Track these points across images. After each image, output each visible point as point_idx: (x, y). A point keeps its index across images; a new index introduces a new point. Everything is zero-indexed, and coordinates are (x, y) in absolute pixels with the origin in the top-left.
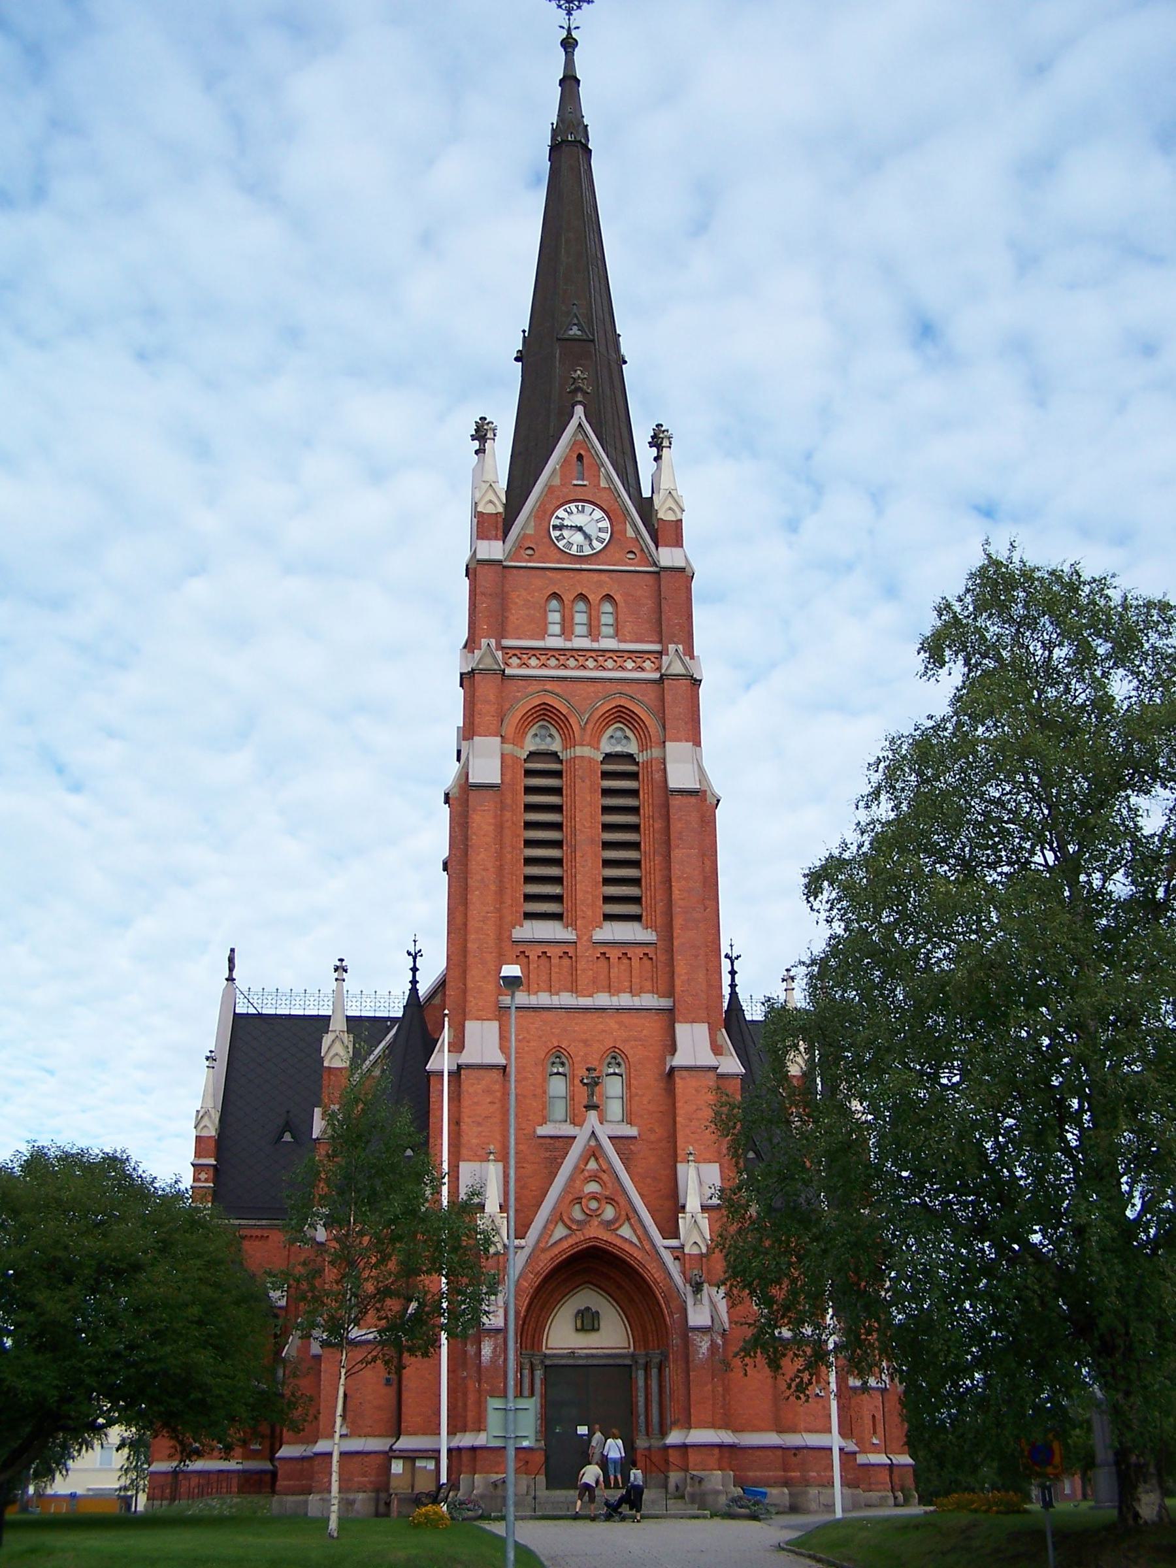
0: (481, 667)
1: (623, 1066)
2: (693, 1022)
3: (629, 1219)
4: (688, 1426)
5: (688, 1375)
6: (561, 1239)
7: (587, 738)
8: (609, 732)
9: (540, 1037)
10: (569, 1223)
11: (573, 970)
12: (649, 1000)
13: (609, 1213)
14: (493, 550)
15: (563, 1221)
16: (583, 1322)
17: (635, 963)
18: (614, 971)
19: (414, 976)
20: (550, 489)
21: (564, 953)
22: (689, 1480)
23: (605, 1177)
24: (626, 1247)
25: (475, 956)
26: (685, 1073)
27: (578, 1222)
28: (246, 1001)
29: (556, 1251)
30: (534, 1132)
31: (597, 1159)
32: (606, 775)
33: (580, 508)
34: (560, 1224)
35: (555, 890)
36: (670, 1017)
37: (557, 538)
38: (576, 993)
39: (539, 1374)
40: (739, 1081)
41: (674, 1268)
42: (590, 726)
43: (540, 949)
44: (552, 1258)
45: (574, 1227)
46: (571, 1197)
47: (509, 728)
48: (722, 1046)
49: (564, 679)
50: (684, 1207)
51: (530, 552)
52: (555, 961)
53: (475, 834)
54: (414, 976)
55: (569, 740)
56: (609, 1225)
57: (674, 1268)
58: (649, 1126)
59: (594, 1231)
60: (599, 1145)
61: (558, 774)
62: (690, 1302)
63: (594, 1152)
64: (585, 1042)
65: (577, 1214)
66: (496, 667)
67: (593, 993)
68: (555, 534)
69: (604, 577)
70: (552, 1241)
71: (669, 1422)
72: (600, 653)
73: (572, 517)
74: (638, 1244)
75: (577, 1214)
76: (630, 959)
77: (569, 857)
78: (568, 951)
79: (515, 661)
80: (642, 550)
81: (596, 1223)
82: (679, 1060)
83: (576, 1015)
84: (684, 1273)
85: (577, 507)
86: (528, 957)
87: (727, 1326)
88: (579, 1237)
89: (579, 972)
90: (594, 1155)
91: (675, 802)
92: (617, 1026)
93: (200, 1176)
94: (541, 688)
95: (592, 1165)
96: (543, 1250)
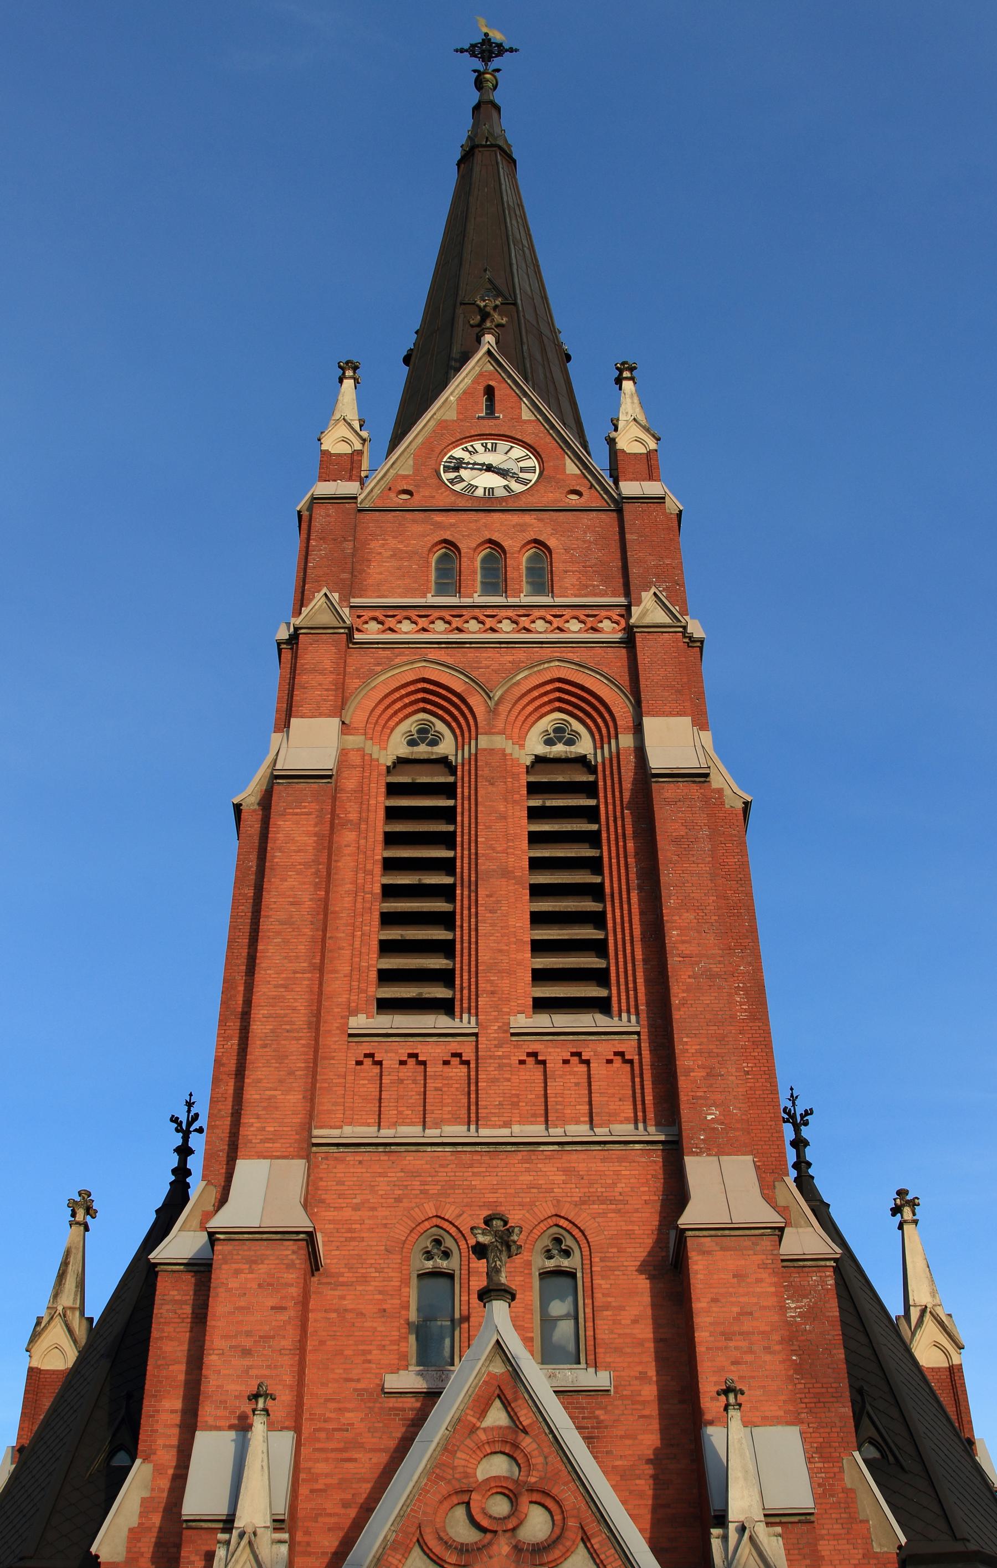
5: (304, 586)
8: (548, 722)
9: (399, 1200)
10: (438, 1549)
15: (422, 1543)
19: (183, 1162)
25: (265, 1046)
31: (506, 1405)
33: (489, 446)
34: (416, 1552)
35: (437, 963)
37: (452, 481)
40: (830, 1273)
46: (444, 1488)
53: (280, 850)
58: (640, 1368)
61: (449, 790)
68: (446, 477)
69: (528, 518)
72: (522, 612)
75: (462, 1531)
83: (476, 1157)
86: (380, 1063)
90: (502, 1397)
91: (663, 793)
92: (560, 1178)
95: (497, 1417)
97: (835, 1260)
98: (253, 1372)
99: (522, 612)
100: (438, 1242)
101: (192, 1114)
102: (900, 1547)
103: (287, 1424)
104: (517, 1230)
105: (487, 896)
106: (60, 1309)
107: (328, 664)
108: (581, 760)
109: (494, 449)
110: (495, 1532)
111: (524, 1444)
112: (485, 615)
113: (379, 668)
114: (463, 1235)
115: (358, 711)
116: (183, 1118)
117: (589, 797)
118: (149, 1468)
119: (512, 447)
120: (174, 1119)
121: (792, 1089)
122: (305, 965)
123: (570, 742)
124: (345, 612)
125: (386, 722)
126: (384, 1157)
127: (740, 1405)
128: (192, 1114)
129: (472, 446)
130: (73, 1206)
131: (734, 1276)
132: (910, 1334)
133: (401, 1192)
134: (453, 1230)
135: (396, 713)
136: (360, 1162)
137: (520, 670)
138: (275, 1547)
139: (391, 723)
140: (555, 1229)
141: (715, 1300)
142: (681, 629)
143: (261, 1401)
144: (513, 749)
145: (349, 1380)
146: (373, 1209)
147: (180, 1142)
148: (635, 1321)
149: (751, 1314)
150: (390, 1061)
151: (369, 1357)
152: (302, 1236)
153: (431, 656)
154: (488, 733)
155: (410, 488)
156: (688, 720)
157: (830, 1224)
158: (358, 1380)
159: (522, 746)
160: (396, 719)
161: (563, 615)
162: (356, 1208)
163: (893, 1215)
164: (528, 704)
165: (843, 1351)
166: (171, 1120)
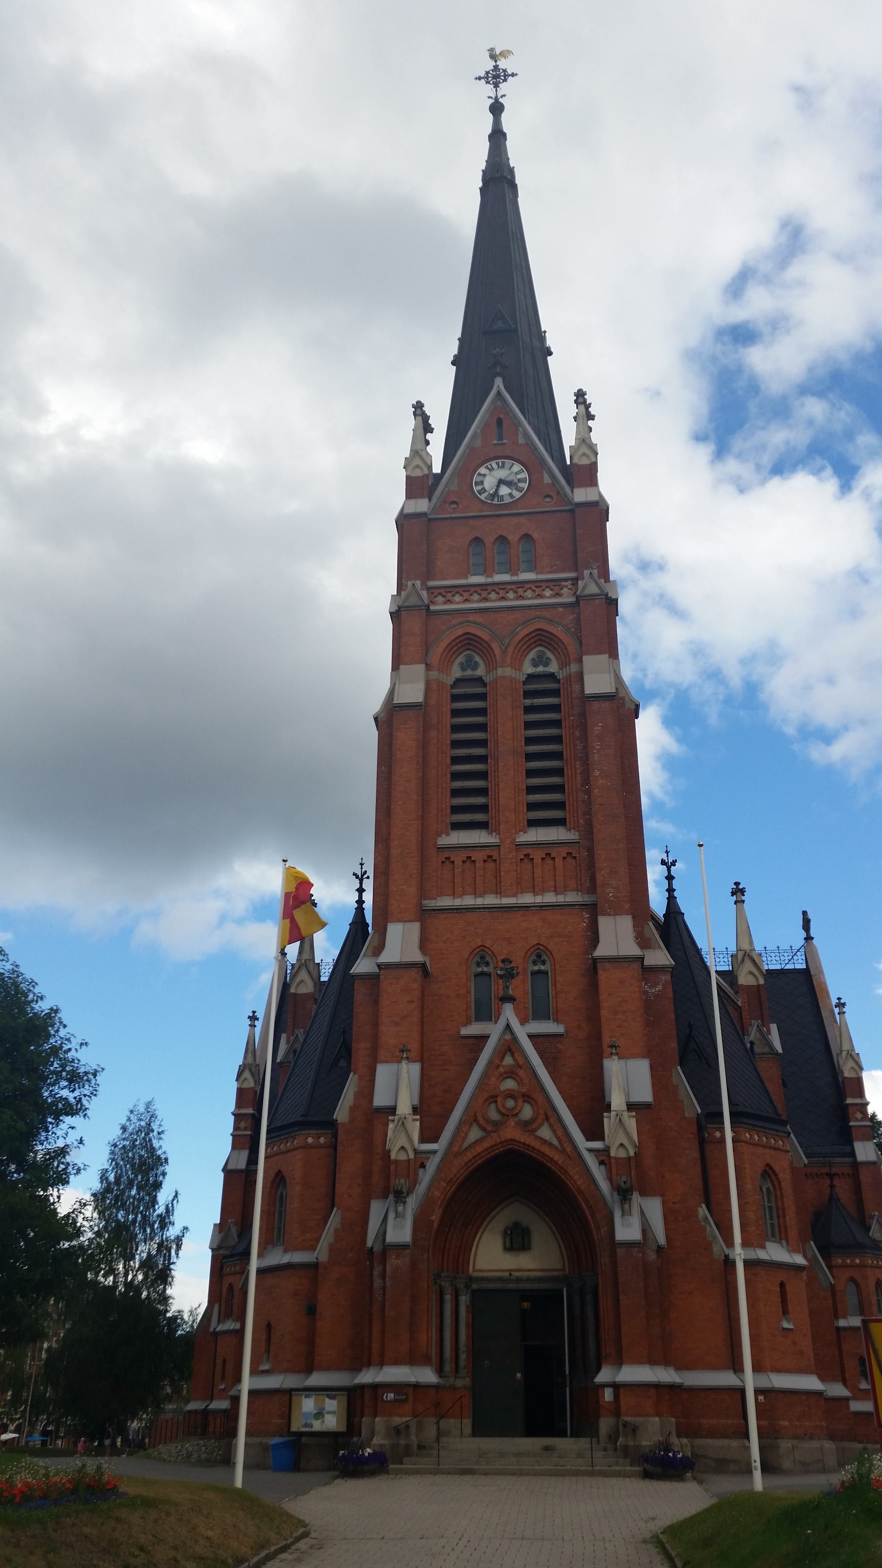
0: (406, 604)
1: (548, 964)
2: (616, 914)
3: (547, 1119)
4: (619, 1362)
6: (474, 1143)
7: (508, 660)
8: (532, 654)
9: (464, 938)
11: (498, 871)
12: (572, 897)
13: (527, 1112)
14: (422, 505)
16: (511, 1240)
17: (559, 862)
18: (538, 872)
19: (360, 896)
20: (471, 450)
21: (488, 856)
22: (621, 1429)
23: (521, 1073)
24: (546, 1150)
26: (607, 965)
27: (495, 1124)
29: (470, 1155)
30: (459, 1032)
31: (512, 1055)
32: (527, 694)
33: (500, 464)
34: (475, 1125)
35: (480, 800)
36: (593, 911)
38: (500, 893)
41: (598, 1173)
42: (511, 649)
43: (464, 855)
44: (466, 1163)
45: (489, 1128)
47: (435, 656)
48: (649, 939)
49: (486, 610)
50: (609, 1106)
51: (454, 506)
52: (479, 864)
55: (492, 664)
56: (528, 1126)
57: (598, 1173)
59: (511, 1132)
60: (515, 1039)
61: (483, 697)
62: (617, 1215)
63: (510, 1045)
65: (493, 1114)
66: (420, 603)
67: (517, 893)
69: (522, 520)
70: (466, 1144)
71: (604, 1354)
73: (494, 473)
74: (559, 1146)
75: (493, 1114)
76: (554, 858)
77: (493, 768)
78: (491, 854)
79: (440, 599)
80: (558, 493)
81: (513, 1124)
82: (602, 951)
84: (610, 1179)
85: (497, 464)
86: (453, 862)
87: (662, 1240)
88: (494, 1139)
89: (502, 873)
93: (240, 1125)
94: (464, 619)
96: (457, 1155)
97: (671, 968)
100: (483, 958)
101: (363, 871)
102: (698, 1114)
103: (417, 1059)
104: (516, 968)
105: (503, 766)
106: (303, 961)
108: (552, 676)
109: (503, 466)
110: (508, 1115)
111: (520, 1074)
112: (500, 589)
114: (495, 955)
115: (435, 656)
116: (359, 874)
117: (556, 697)
118: (356, 1076)
119: (513, 464)
120: (355, 874)
121: (667, 847)
122: (414, 816)
124: (424, 594)
125: (450, 659)
126: (457, 915)
127: (618, 1053)
128: (363, 871)
129: (490, 464)
131: (619, 982)
132: (737, 966)
133: (465, 933)
134: (490, 952)
135: (454, 653)
136: (446, 918)
138: (414, 1122)
139: (452, 659)
142: (604, 597)
143: (405, 1053)
144: (516, 673)
147: (358, 886)
149: (627, 1002)
150: (458, 862)
151: (453, 1019)
152: (418, 966)
153: (471, 618)
155: (456, 500)
156: (607, 655)
157: (683, 926)
158: (448, 1030)
159: (520, 670)
160: (454, 656)
161: (541, 586)
163: (732, 896)
164: (523, 645)
165: (674, 1015)
166: (354, 875)
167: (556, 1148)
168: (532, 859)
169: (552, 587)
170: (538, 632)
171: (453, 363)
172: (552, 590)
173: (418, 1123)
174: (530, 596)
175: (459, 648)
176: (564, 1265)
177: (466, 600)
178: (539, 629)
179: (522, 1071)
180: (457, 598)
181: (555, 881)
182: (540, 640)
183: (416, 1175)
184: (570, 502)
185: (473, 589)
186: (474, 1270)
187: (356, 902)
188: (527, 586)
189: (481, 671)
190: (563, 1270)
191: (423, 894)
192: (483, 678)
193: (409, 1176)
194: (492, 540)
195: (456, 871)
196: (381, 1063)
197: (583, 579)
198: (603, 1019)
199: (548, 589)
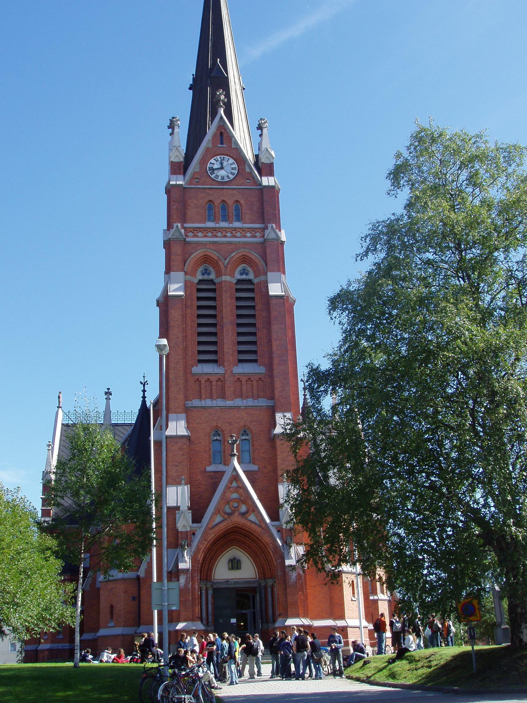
1: (250, 435)
7: (228, 272)
8: (240, 268)
17: (255, 383)
18: (244, 388)
19: (144, 394)
20: (207, 149)
27: (228, 514)
28: (67, 417)
32: (238, 290)
33: (222, 158)
39: (210, 592)
43: (206, 378)
51: (197, 180)
54: (144, 394)
59: (237, 519)
61: (214, 290)
64: (230, 423)
70: (214, 524)
76: (252, 381)
79: (190, 234)
89: (226, 388)
98: (178, 471)
99: (234, 229)
107: (179, 252)
108: (250, 281)
113: (193, 251)
123: (247, 274)
130: (106, 393)
137: (233, 252)
140: (244, 429)
141: (282, 452)
145: (198, 468)
146: (201, 424)
148: (263, 453)
154: (225, 275)
159: (234, 277)
162: (197, 424)
167: (258, 525)
168: (241, 381)
169: (251, 232)
170: (244, 257)
171: (190, 89)
172: (251, 233)
173: (191, 514)
174: (239, 236)
175: (201, 263)
176: (256, 576)
177: (205, 236)
178: (244, 255)
179: (241, 490)
180: (200, 234)
181: (253, 392)
182: (244, 261)
183: (191, 538)
184: (260, 184)
185: (209, 230)
186: (214, 579)
187: (142, 397)
188: (238, 230)
189: (212, 276)
190: (256, 578)
191: (186, 399)
192: (214, 280)
193: (187, 539)
194: (219, 202)
195: (202, 386)
196: (170, 484)
197: (267, 229)
198: (278, 464)
199: (249, 232)
